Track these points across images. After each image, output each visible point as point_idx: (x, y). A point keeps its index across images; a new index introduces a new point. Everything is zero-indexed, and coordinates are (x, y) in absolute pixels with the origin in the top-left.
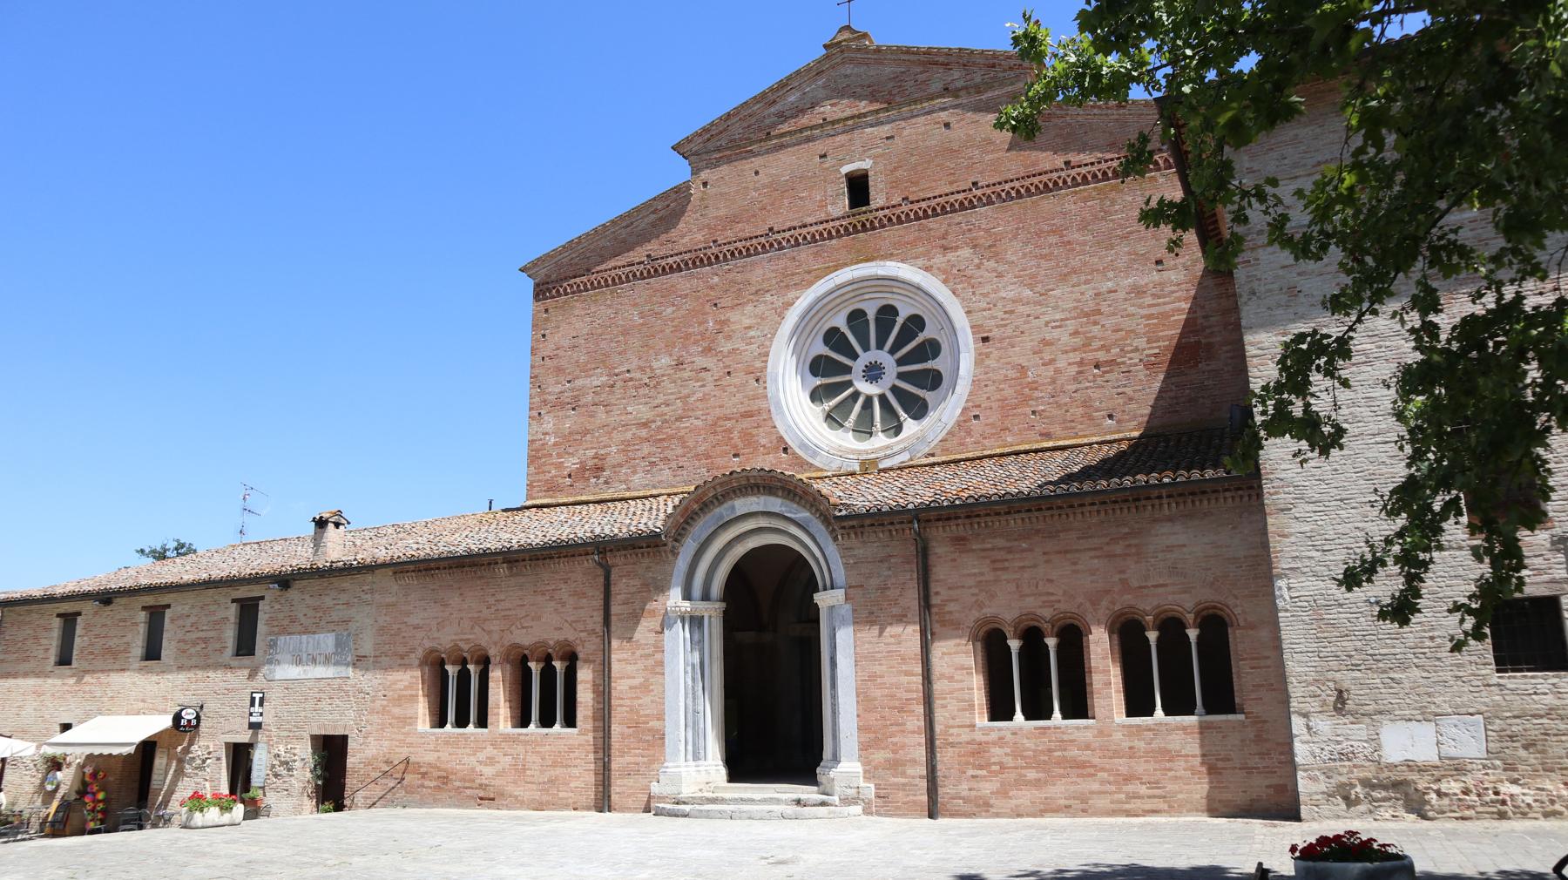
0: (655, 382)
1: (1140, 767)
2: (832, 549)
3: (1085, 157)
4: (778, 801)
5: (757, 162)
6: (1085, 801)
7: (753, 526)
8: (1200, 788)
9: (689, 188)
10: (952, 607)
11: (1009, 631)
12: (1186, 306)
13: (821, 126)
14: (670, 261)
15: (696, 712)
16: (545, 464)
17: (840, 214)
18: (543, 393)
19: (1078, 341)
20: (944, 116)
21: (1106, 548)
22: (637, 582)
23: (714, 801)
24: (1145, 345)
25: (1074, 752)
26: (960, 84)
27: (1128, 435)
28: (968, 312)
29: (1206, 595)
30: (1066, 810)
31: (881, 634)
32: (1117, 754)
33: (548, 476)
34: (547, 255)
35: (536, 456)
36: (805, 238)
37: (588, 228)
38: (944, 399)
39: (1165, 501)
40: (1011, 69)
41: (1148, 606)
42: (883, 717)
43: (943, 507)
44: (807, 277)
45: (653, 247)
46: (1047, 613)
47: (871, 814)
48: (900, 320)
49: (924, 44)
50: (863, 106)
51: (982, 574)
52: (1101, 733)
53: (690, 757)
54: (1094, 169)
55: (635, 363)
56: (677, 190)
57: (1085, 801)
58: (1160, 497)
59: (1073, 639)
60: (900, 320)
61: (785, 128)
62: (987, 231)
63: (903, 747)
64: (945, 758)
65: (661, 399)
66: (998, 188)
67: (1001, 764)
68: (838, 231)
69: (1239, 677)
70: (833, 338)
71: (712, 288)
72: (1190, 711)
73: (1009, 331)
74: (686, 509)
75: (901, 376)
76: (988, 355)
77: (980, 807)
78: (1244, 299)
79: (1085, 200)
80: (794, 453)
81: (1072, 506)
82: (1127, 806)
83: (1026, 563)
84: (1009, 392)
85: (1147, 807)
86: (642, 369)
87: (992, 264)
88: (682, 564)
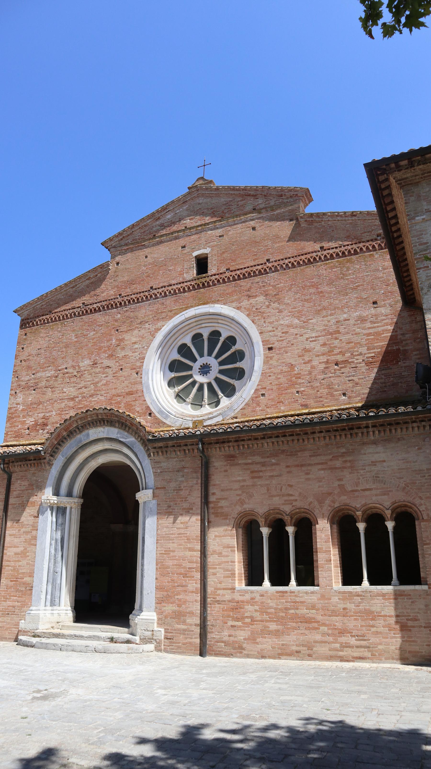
0: (80, 374)
1: (351, 624)
2: (147, 462)
3: (332, 244)
4: (98, 638)
5: (147, 251)
6: (310, 648)
7: (101, 449)
8: (395, 641)
9: (108, 265)
10: (223, 503)
11: (261, 521)
12: (391, 328)
13: (184, 230)
14: (95, 306)
15: (55, 572)
16: (16, 422)
17: (191, 278)
18: (19, 380)
19: (326, 349)
20: (252, 223)
21: (330, 463)
22: (26, 483)
23: (57, 636)
24: (366, 351)
25: (303, 611)
26: (261, 206)
27: (355, 405)
28: (261, 333)
29: (400, 497)
30: (295, 654)
31: (174, 522)
32: (334, 613)
33: (16, 429)
34: (29, 303)
35: (11, 417)
36: (170, 292)
37: (52, 288)
38: (245, 385)
39: (371, 429)
40: (291, 197)
41: (358, 504)
42: (173, 580)
43: (218, 433)
44: (170, 314)
45: (87, 299)
46: (287, 509)
47: (160, 650)
48: (222, 339)
49: (242, 184)
50: (207, 219)
51: (244, 481)
52: (323, 597)
53: (48, 603)
54: (337, 250)
55: (71, 363)
56: (102, 266)
57: (310, 648)
58: (367, 427)
59: (306, 527)
60: (222, 339)
61: (164, 232)
62: (274, 286)
63: (185, 602)
64: (213, 611)
65: (82, 384)
66: (281, 262)
67: (251, 617)
68: (189, 288)
69: (424, 557)
70: (183, 350)
71: (116, 321)
72: (388, 582)
73: (284, 344)
74: (59, 435)
75: (221, 372)
76: (271, 358)
77: (236, 650)
78: (425, 290)
79: (332, 268)
80: (155, 416)
81: (306, 434)
82: (341, 653)
83: (275, 473)
84: (283, 380)
85: (356, 654)
86: (74, 367)
87: (276, 305)
88: (54, 471)
